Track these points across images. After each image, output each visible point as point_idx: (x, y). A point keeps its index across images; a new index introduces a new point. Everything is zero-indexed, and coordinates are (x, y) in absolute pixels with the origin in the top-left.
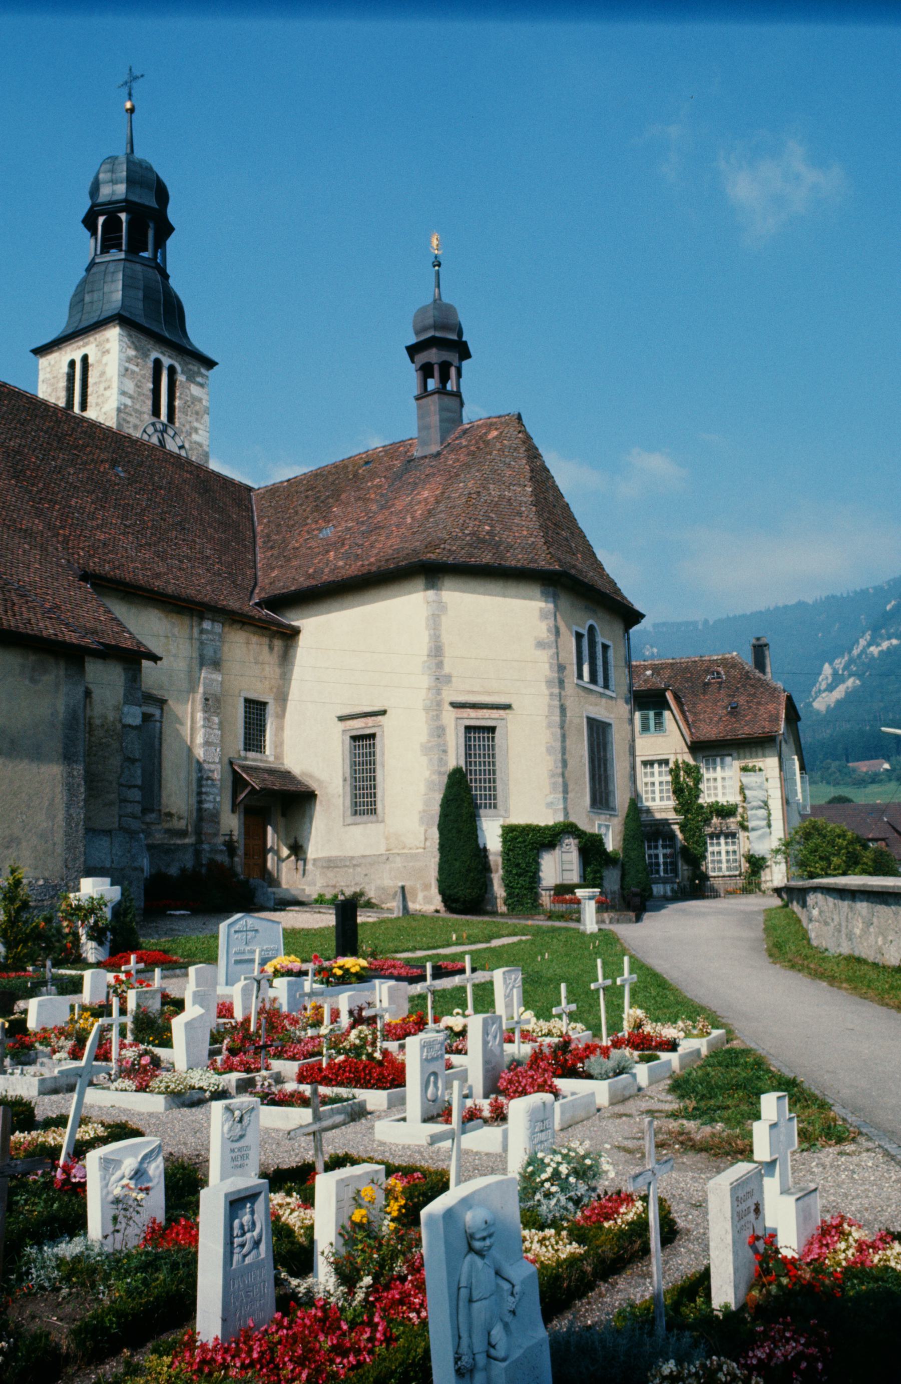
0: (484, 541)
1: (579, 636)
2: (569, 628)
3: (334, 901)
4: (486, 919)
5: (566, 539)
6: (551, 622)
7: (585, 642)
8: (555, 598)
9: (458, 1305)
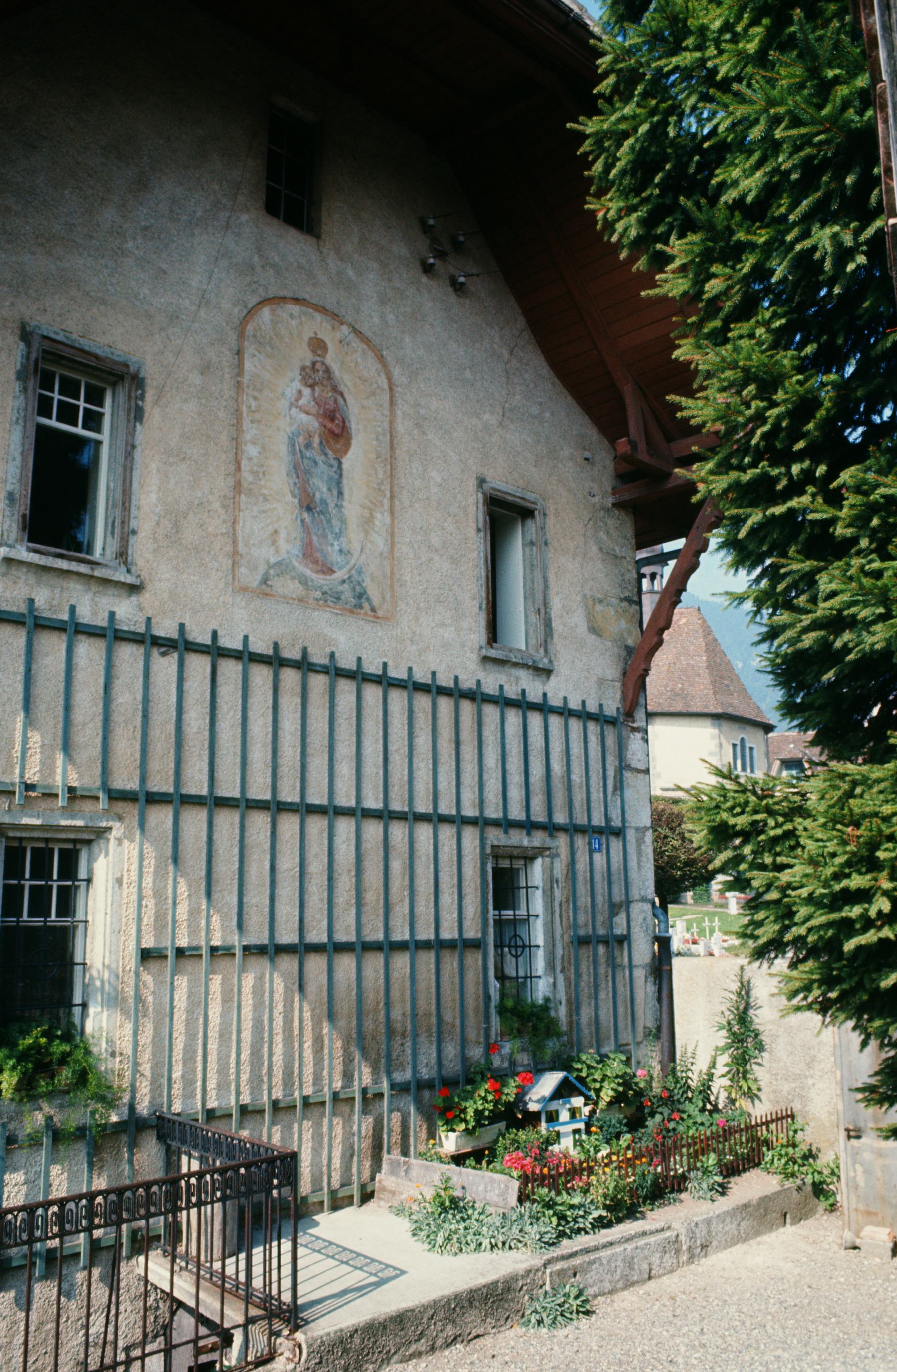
0: (677, 694)
1: (734, 745)
2: (727, 740)
3: (624, 826)
4: (681, 906)
5: (727, 686)
6: (717, 741)
7: (738, 748)
8: (719, 726)
9: (387, 868)
